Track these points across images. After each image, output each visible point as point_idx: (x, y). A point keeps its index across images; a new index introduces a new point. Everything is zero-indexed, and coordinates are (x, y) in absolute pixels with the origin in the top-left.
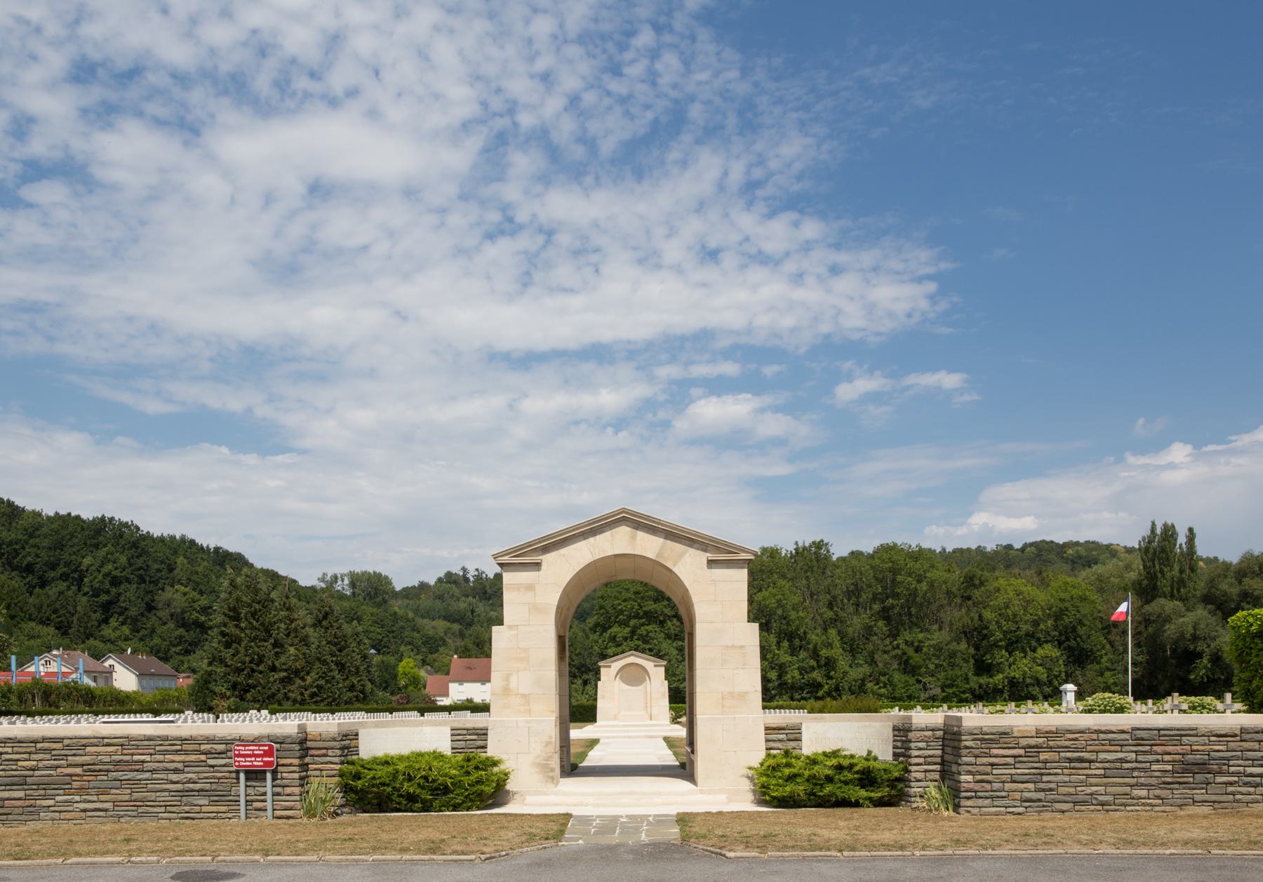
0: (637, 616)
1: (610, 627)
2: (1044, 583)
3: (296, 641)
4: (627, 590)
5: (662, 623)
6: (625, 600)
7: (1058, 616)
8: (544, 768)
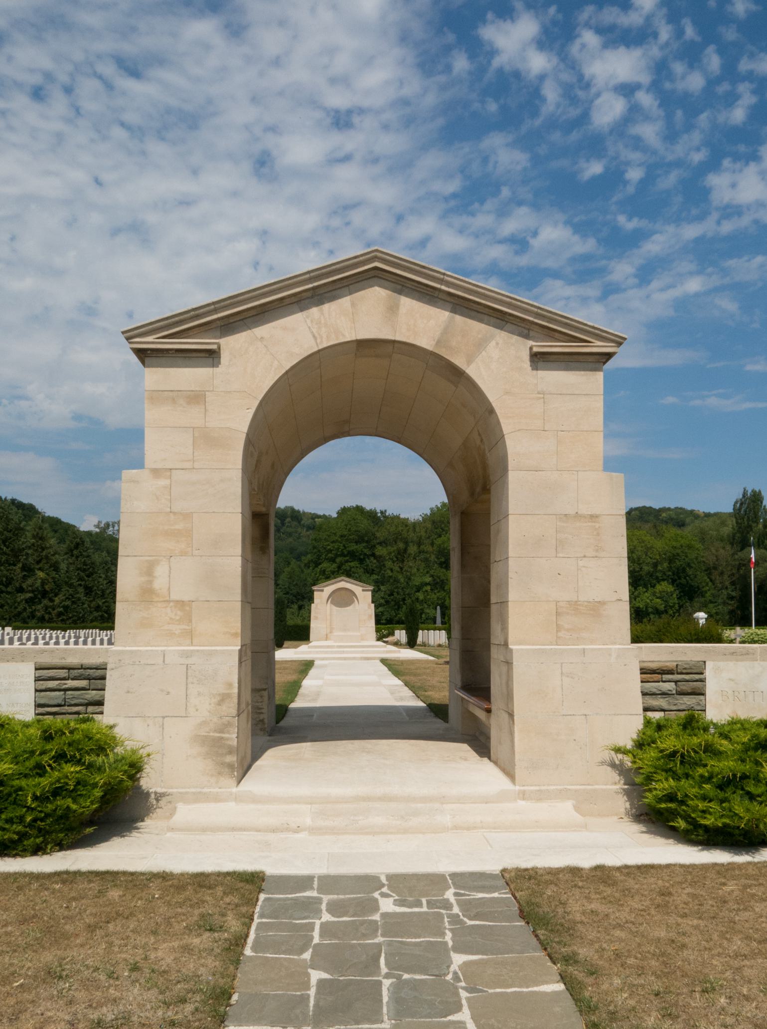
0: (343, 555)
1: (320, 564)
2: (659, 535)
3: (46, 567)
4: (335, 534)
5: (361, 561)
6: (333, 542)
7: (671, 561)
8: (213, 745)
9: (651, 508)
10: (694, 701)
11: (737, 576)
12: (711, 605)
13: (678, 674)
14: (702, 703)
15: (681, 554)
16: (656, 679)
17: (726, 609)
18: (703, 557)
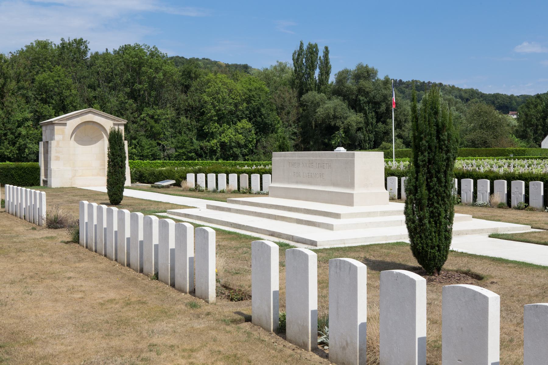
15: (256, 96)
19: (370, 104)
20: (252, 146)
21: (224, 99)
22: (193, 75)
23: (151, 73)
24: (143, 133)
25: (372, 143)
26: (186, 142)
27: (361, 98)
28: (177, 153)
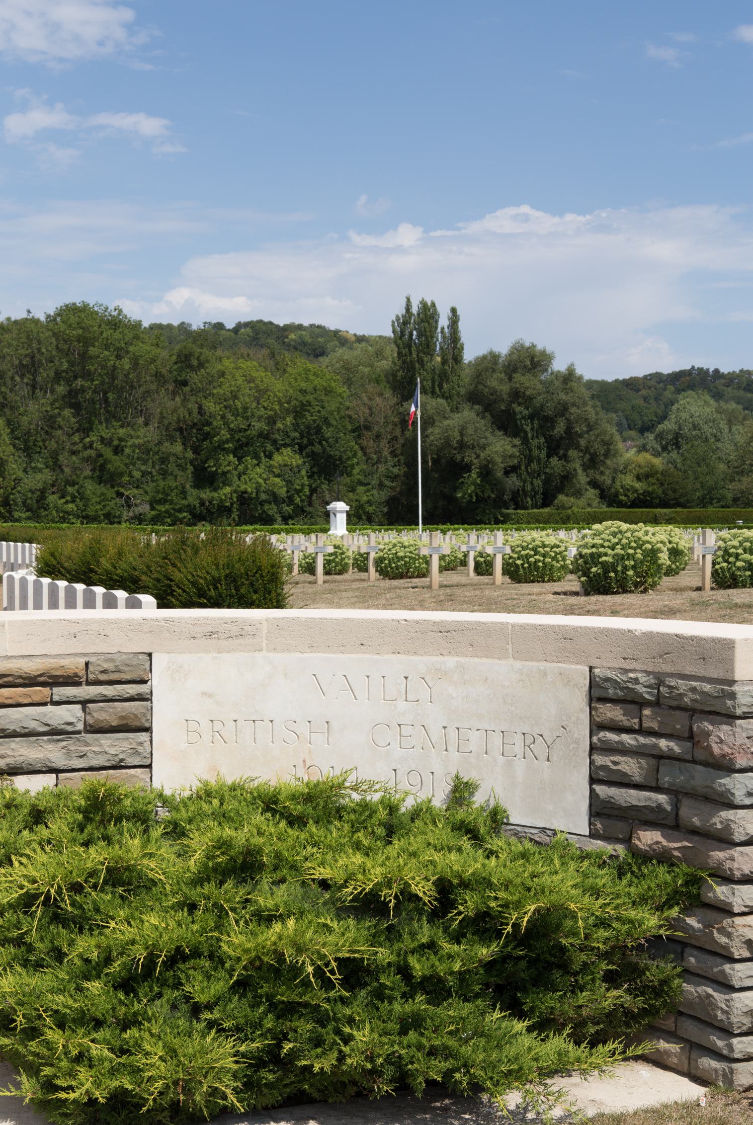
2: (280, 369)
9: (271, 323)
10: (126, 745)
11: (401, 441)
12: (360, 489)
13: (89, 683)
14: (145, 750)
15: (314, 403)
16: (36, 699)
17: (384, 495)
18: (348, 408)
19: (536, 422)
20: (302, 501)
21: (245, 409)
22: (195, 362)
23: (106, 360)
24: (88, 472)
25: (539, 497)
26: (172, 490)
27: (518, 409)
28: (153, 513)
